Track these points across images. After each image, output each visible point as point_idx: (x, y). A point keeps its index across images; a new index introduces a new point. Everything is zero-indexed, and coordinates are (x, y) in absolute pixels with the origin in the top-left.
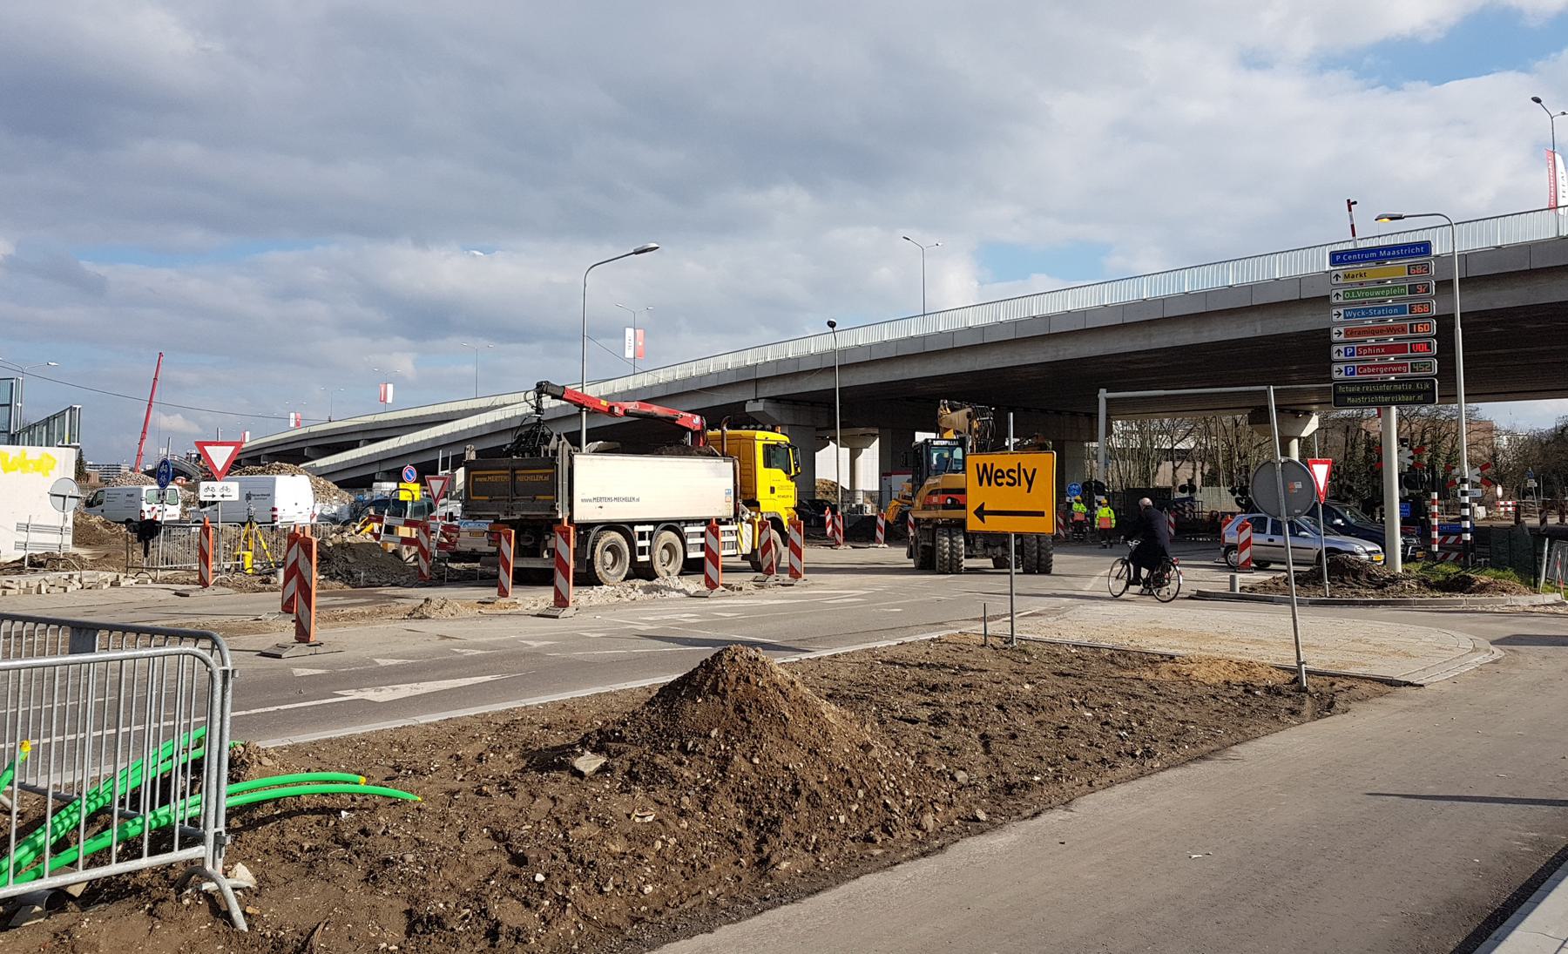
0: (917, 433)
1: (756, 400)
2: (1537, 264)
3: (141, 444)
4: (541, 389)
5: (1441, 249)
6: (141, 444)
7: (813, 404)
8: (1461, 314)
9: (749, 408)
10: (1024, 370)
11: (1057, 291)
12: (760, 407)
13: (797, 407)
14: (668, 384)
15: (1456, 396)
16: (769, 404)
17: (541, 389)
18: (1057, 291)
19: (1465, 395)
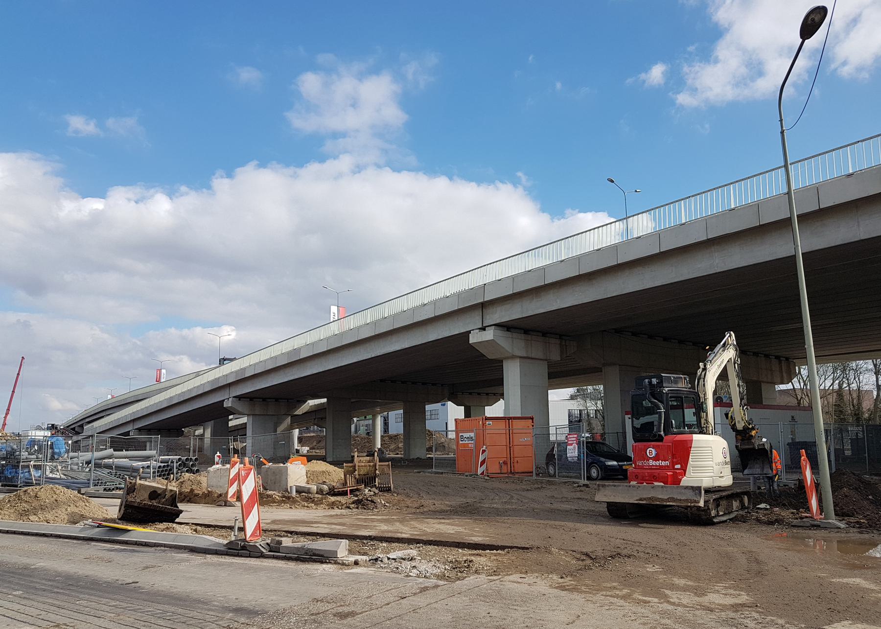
0: (463, 407)
1: (483, 329)
2: (303, 355)
3: (5, 417)
4: (48, 424)
5: (853, 167)
6: (5, 417)
7: (544, 334)
8: (802, 254)
9: (473, 339)
10: (431, 343)
11: (459, 275)
12: (489, 335)
13: (529, 337)
14: (375, 323)
15: (806, 358)
16: (500, 332)
17: (48, 424)
18: (467, 272)
19: (815, 357)
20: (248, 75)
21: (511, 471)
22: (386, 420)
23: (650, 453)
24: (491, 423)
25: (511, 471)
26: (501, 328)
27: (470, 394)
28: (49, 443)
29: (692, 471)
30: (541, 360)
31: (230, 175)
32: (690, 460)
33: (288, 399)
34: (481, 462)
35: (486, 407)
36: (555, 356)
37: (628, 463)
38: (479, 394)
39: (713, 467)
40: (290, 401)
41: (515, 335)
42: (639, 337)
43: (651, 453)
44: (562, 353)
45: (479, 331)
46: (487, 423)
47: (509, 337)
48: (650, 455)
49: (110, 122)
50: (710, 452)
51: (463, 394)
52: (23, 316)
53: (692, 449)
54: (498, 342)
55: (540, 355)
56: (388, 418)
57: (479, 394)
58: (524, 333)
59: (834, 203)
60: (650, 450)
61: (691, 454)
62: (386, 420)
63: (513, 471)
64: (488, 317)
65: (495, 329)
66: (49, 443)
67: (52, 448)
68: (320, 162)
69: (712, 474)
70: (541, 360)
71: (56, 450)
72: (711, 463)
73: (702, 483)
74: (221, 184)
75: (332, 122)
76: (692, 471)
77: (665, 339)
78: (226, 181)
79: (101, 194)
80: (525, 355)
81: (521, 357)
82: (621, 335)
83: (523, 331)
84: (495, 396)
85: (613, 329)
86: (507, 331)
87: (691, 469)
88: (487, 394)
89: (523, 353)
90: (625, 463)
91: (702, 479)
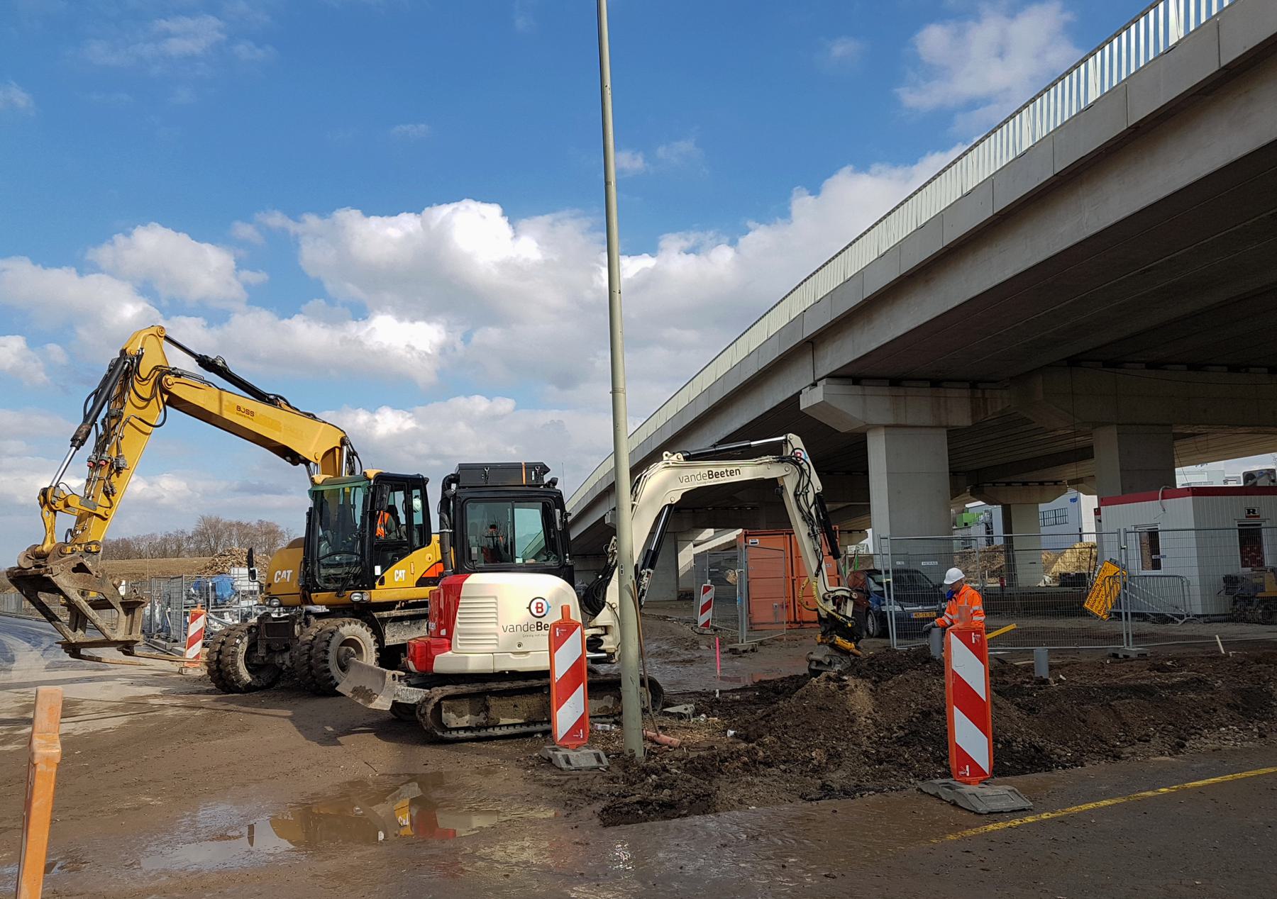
13: (901, 391)
16: (837, 389)
20: (843, 49)
21: (795, 619)
22: (988, 529)
23: (537, 608)
24: (757, 541)
25: (795, 619)
26: (837, 381)
27: (1008, 484)
28: (210, 584)
29: (459, 641)
30: (931, 427)
31: (815, 191)
32: (457, 620)
33: (693, 509)
34: (702, 607)
35: (1040, 505)
36: (961, 419)
37: (926, 608)
38: (1025, 484)
39: (497, 635)
40: (696, 511)
41: (869, 390)
42: (1166, 369)
43: (541, 608)
44: (974, 413)
45: (810, 389)
46: (750, 541)
47: (886, 396)
48: (538, 612)
49: (661, 151)
50: (494, 605)
51: (994, 485)
52: (553, 415)
53: (461, 601)
54: (833, 404)
55: (926, 419)
56: (992, 524)
57: (1025, 484)
58: (931, 387)
59: (1245, 47)
60: (537, 604)
61: (459, 611)
62: (988, 529)
63: (798, 620)
64: (819, 365)
65: (827, 384)
66: (210, 584)
67: (214, 589)
68: (942, 151)
69: (495, 647)
70: (931, 427)
71: (219, 593)
72: (494, 626)
73: (466, 664)
74: (802, 204)
75: (966, 85)
76: (459, 641)
77: (1234, 368)
78: (810, 199)
79: (653, 250)
80: (892, 422)
81: (886, 426)
82: (1117, 370)
83: (887, 382)
84: (1056, 486)
85: (1064, 360)
86: (854, 384)
87: (458, 637)
88: (1041, 483)
89: (890, 420)
90: (920, 607)
91: (466, 657)
